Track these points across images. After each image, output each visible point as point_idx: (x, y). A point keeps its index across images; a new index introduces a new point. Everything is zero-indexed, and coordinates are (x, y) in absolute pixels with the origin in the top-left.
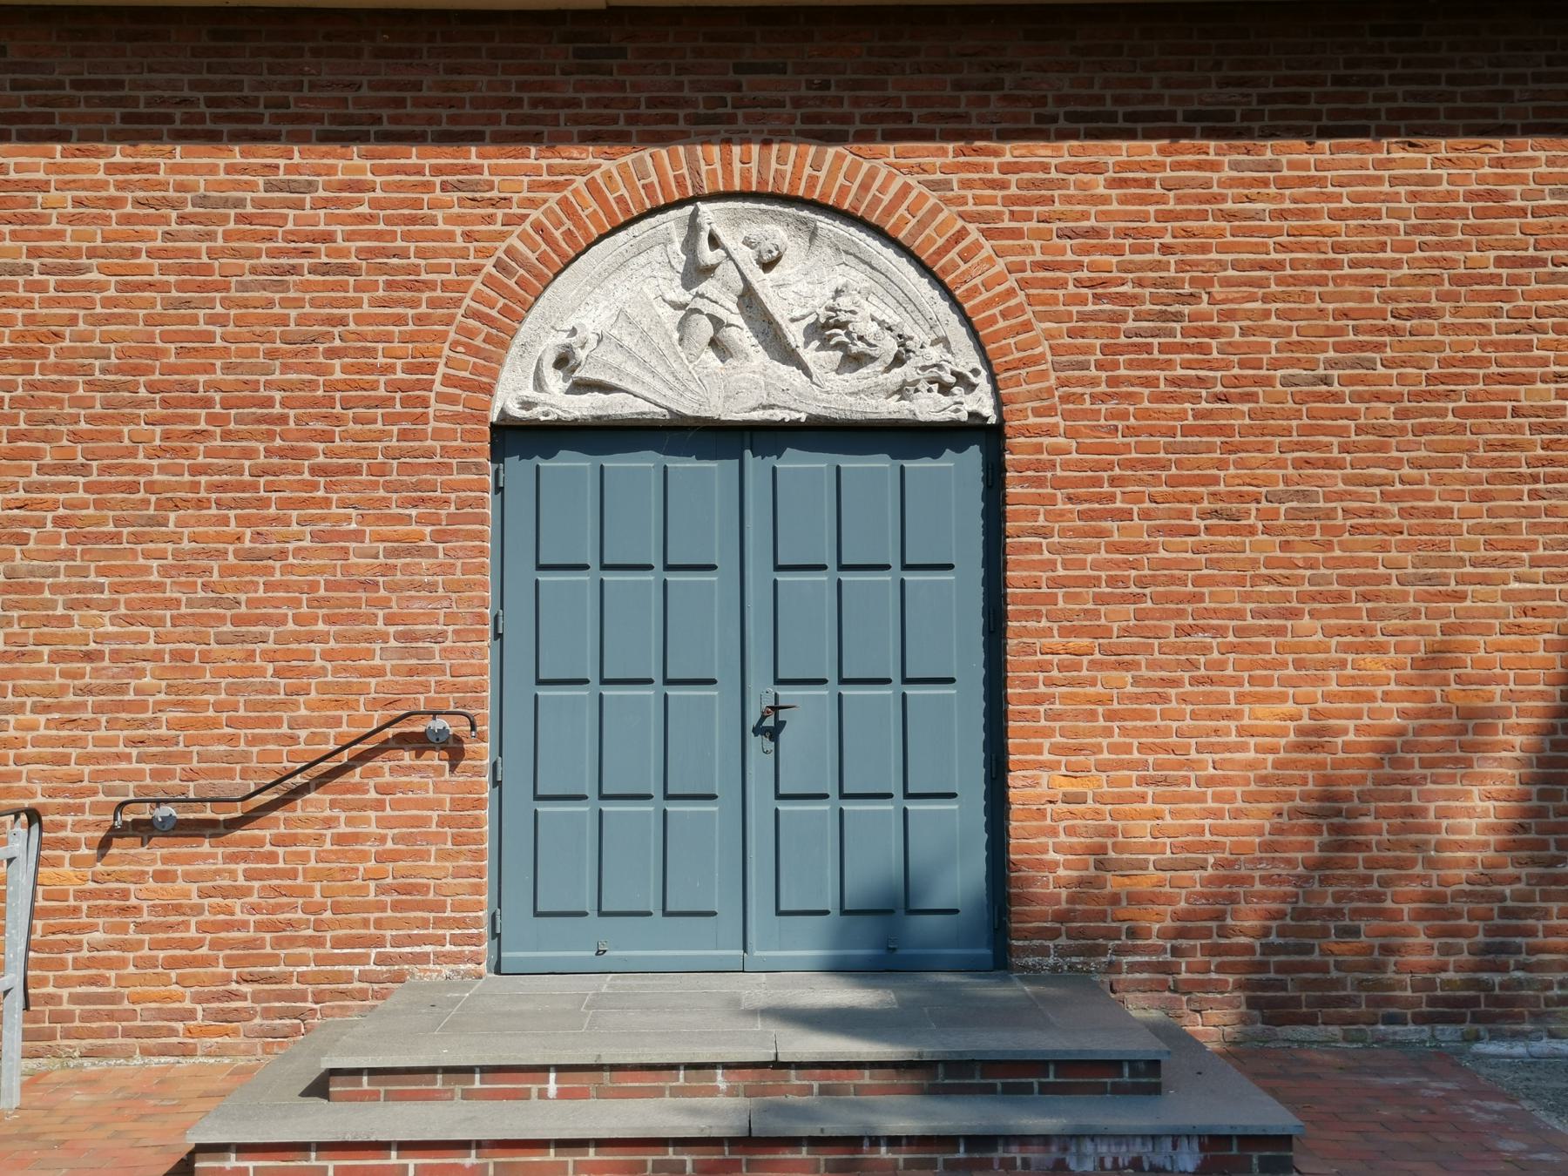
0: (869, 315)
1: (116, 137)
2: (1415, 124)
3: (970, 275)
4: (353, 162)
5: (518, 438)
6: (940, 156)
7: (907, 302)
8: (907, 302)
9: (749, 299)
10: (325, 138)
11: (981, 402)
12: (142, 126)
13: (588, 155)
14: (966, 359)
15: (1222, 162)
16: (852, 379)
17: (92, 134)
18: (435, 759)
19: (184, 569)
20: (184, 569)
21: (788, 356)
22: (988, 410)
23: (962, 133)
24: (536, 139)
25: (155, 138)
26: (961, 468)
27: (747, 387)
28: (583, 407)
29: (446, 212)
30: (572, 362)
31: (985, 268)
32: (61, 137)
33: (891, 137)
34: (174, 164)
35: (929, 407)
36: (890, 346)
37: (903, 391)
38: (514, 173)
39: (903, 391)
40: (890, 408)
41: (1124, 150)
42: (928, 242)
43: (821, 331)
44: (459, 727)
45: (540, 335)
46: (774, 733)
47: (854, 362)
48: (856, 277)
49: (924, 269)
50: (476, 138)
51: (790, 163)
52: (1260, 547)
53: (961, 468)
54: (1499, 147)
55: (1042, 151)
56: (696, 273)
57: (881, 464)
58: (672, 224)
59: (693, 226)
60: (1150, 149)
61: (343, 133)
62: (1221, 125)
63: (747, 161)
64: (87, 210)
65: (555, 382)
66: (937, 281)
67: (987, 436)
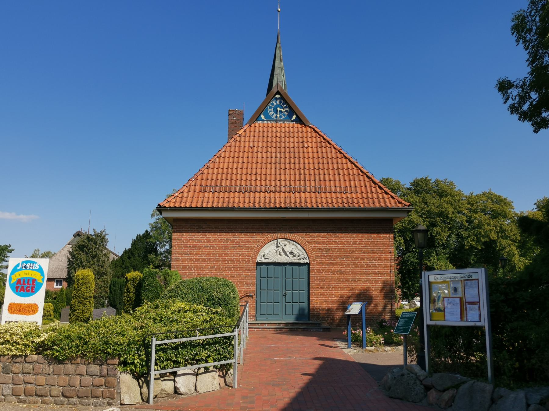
0: (296, 251)
2: (353, 232)
4: (242, 235)
5: (259, 264)
7: (300, 250)
8: (300, 250)
9: (283, 250)
11: (307, 261)
12: (221, 231)
14: (306, 256)
15: (333, 235)
17: (215, 232)
18: (250, 298)
21: (287, 256)
23: (305, 232)
27: (283, 259)
31: (308, 246)
34: (224, 235)
35: (302, 261)
37: (299, 259)
39: (299, 259)
40: (298, 261)
42: (302, 244)
43: (290, 253)
44: (253, 294)
45: (261, 253)
46: (285, 296)
47: (294, 256)
48: (294, 247)
49: (301, 246)
50: (255, 233)
51: (288, 235)
54: (362, 234)
55: (314, 234)
56: (277, 247)
57: (297, 267)
58: (275, 241)
59: (277, 242)
61: (241, 232)
63: (283, 235)
65: (263, 258)
67: (308, 264)
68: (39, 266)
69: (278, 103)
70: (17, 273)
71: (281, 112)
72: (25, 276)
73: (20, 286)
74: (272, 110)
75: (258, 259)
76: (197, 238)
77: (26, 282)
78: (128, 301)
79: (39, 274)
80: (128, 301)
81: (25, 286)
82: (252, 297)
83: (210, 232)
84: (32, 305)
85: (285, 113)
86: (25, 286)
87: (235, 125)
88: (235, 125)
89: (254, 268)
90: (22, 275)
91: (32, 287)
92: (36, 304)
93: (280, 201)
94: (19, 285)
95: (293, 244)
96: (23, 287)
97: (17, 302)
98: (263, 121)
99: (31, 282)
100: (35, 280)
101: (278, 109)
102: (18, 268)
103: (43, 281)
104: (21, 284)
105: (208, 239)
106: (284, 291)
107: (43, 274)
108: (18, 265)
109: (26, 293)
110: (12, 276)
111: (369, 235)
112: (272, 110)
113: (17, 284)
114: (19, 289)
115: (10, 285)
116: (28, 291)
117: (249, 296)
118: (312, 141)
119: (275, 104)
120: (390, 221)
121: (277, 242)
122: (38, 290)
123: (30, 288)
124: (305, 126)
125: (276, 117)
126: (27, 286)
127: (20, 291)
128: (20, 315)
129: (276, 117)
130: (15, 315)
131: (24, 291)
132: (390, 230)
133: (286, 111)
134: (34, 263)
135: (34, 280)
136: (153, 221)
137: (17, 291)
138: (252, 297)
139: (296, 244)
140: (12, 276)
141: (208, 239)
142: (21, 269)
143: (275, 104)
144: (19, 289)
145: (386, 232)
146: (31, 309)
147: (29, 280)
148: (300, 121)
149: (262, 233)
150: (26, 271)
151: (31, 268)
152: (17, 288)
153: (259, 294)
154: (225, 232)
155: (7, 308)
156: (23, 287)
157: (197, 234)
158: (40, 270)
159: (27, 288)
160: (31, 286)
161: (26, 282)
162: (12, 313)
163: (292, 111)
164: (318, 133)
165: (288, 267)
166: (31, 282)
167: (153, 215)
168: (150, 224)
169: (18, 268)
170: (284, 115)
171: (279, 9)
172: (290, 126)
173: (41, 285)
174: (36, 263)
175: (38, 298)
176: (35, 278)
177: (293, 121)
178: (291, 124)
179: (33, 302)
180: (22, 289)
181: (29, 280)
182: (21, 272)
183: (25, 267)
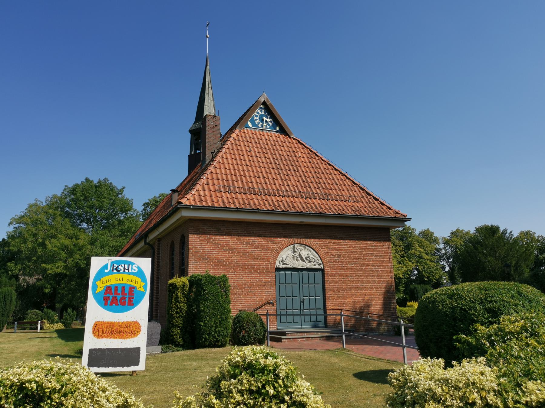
0: (311, 256)
1: (237, 236)
2: (359, 239)
3: (320, 253)
4: (261, 239)
5: (278, 269)
6: (317, 240)
7: (314, 256)
8: (314, 256)
9: (300, 255)
10: (258, 236)
11: (322, 266)
12: (239, 235)
13: (284, 239)
14: (320, 262)
15: (342, 242)
16: (310, 264)
17: (234, 235)
18: (271, 305)
19: (245, 284)
20: (245, 284)
21: (304, 261)
22: (398, 307)
23: (319, 238)
24: (279, 237)
25: (241, 236)
26: (319, 273)
27: (300, 264)
28: (284, 266)
29: (270, 245)
30: (34, 216)
31: (322, 252)
32: (231, 235)
33: (313, 238)
34: (243, 238)
35: (318, 267)
36: (313, 260)
37: (315, 265)
38: (277, 240)
39: (315, 265)
40: (314, 267)
41: (333, 241)
42: (317, 250)
43: (306, 258)
44: (274, 302)
45: (280, 258)
46: (303, 302)
47: (310, 262)
48: (309, 252)
49: (316, 252)
50: (273, 237)
51: (303, 241)
52: (348, 282)
53: (319, 273)
54: (366, 242)
55: (326, 240)
56: (294, 252)
57: (312, 273)
58: (292, 246)
59: (294, 247)
60: (336, 241)
61: (260, 236)
62: (343, 239)
63: (299, 240)
64: (234, 243)
65: (281, 263)
66: (317, 253)
67: (322, 270)
68: (138, 267)
69: (263, 113)
70: (105, 279)
71: (266, 121)
72: (118, 282)
73: (111, 297)
74: (257, 118)
75: (277, 264)
76: (216, 240)
77: (119, 291)
78: (177, 313)
79: (139, 280)
80: (177, 313)
81: (119, 297)
82: (273, 304)
83: (229, 235)
84: (130, 323)
85: (270, 123)
86: (119, 297)
87: (213, 130)
88: (213, 130)
89: (273, 273)
90: (112, 280)
91: (129, 298)
92: (136, 322)
93: (298, 204)
94: (108, 295)
95: (308, 250)
96: (115, 299)
97: (107, 320)
98: (250, 128)
99: (127, 291)
100: (134, 287)
101: (265, 118)
102: (106, 271)
103: (146, 290)
104: (111, 294)
105: (227, 243)
106: (302, 297)
107: (143, 279)
108: (106, 267)
109: (120, 307)
110: (98, 283)
111: (371, 242)
112: (257, 118)
113: (105, 294)
114: (109, 302)
115: (95, 295)
116: (123, 304)
117: (270, 303)
118: (301, 153)
119: (260, 113)
120: (386, 230)
121: (294, 247)
122: (138, 302)
123: (127, 300)
124: (290, 137)
125: (262, 126)
126: (121, 296)
127: (111, 304)
128: (112, 340)
129: (262, 126)
130: (105, 339)
131: (117, 304)
132: (388, 239)
133: (271, 122)
134: (129, 263)
135: (132, 289)
136: (11, 229)
137: (106, 304)
138: (273, 304)
139: (311, 249)
140: (98, 283)
141: (227, 243)
142: (108, 274)
143: (260, 113)
144: (109, 302)
145: (385, 241)
146: (130, 330)
147: (123, 288)
148: (283, 131)
149: (280, 238)
150: (119, 276)
151: (127, 271)
152: (106, 299)
153: (278, 300)
154: (244, 236)
155: (91, 330)
156: (115, 299)
157: (215, 237)
158: (140, 274)
159: (121, 299)
160: (127, 296)
161: (119, 291)
162: (99, 337)
163: (276, 122)
164: (303, 145)
165: (304, 273)
166: (127, 291)
167: (10, 224)
168: (7, 232)
169: (106, 271)
170: (269, 125)
171: (208, 36)
172: (275, 135)
173: (143, 294)
174: (133, 264)
175: (140, 313)
176: (133, 284)
177: (277, 132)
178: (276, 134)
179: (131, 320)
180: (114, 301)
181: (123, 288)
182: (112, 277)
183: (116, 269)
